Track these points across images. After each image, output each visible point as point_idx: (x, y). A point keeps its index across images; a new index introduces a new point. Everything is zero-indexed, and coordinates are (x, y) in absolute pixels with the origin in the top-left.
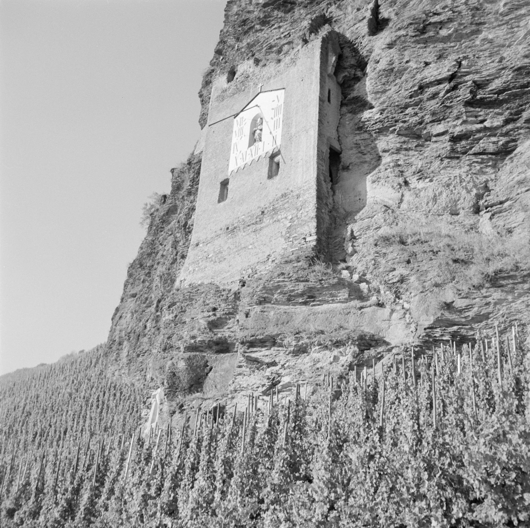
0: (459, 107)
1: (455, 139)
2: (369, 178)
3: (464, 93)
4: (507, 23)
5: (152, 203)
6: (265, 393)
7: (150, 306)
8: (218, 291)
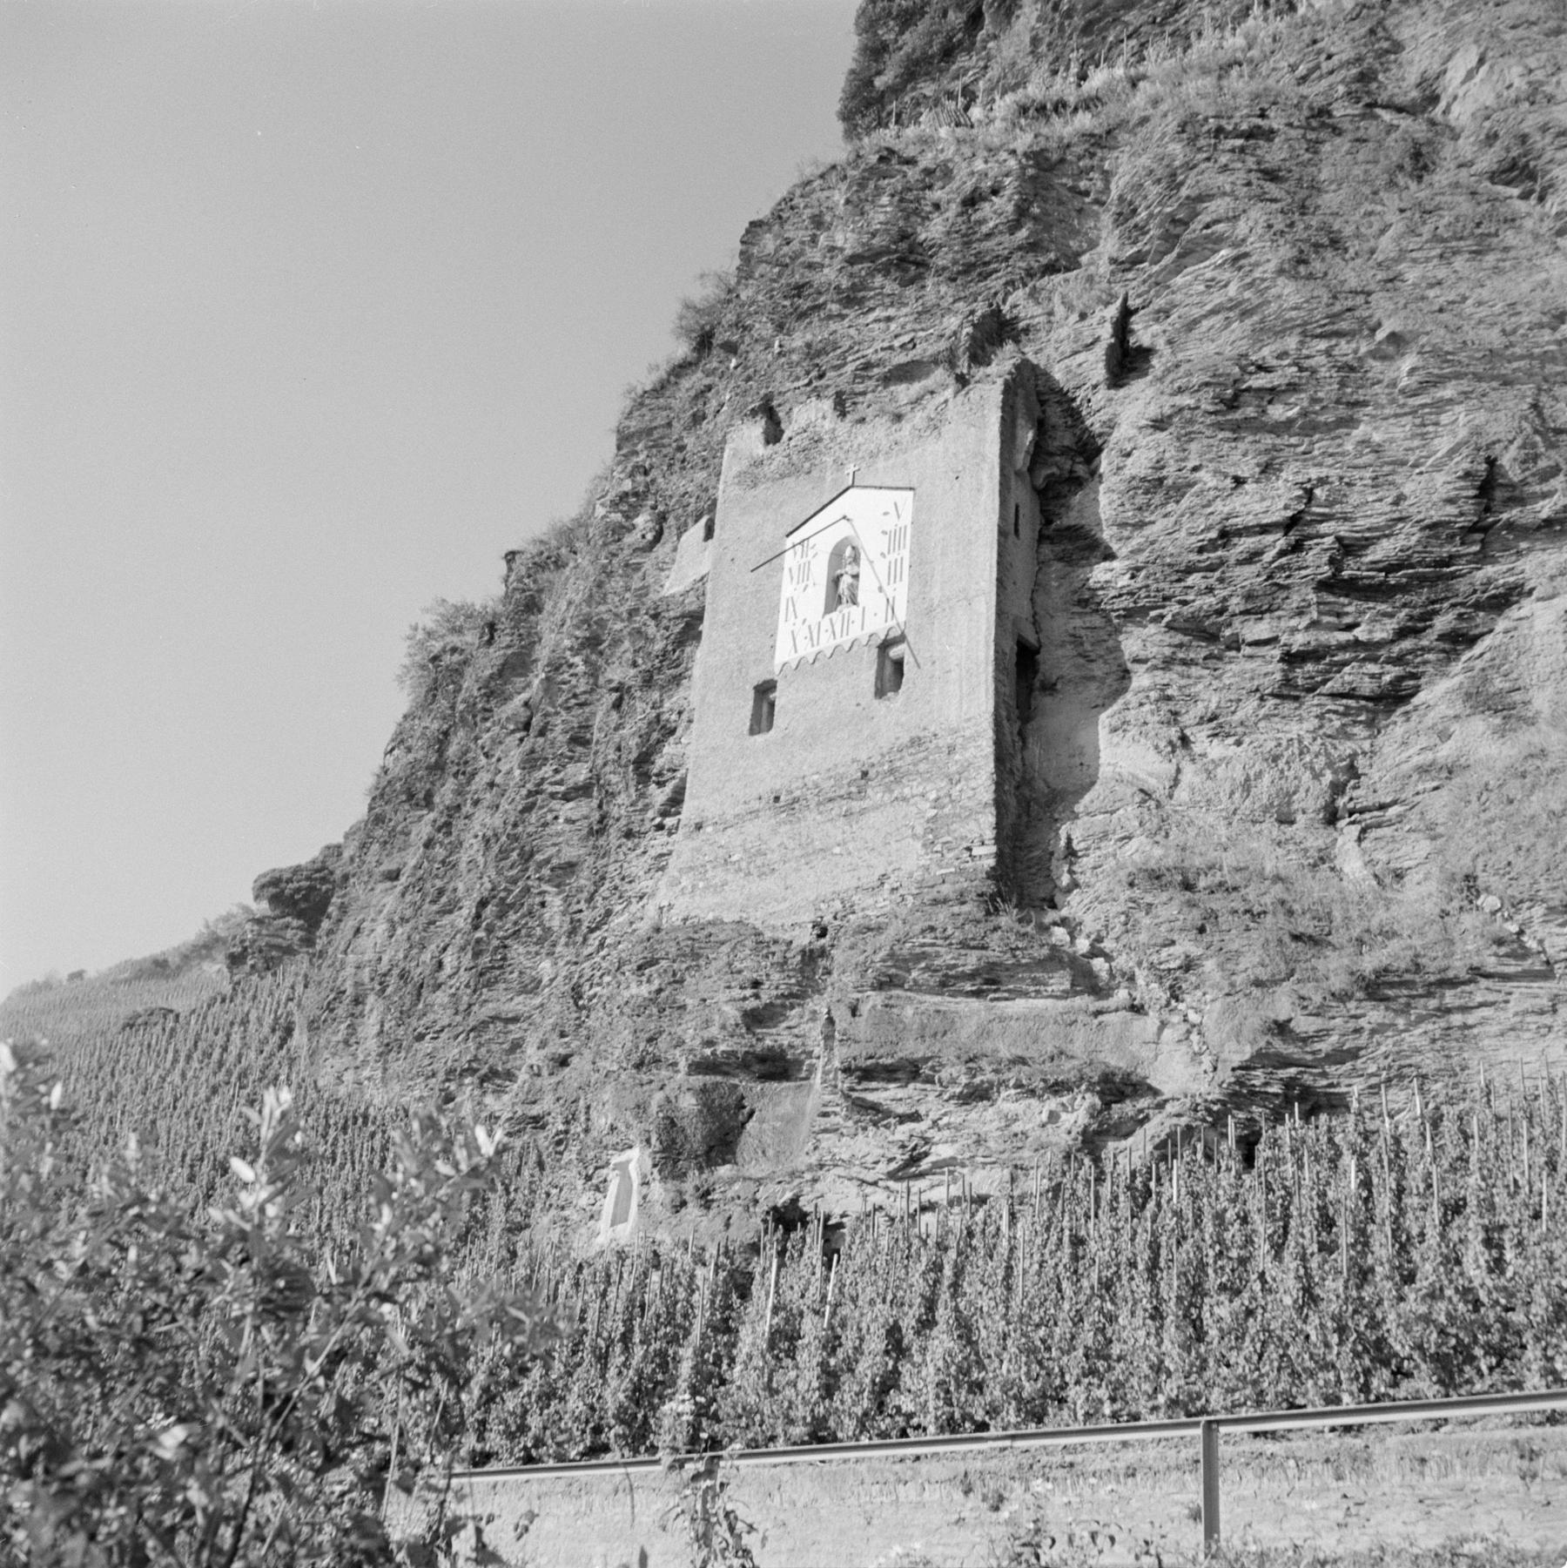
0: (1304, 591)
1: (1292, 659)
2: (1105, 719)
3: (1316, 561)
4: (1413, 412)
5: (431, 625)
6: (892, 1176)
7: (451, 912)
8: (762, 945)
